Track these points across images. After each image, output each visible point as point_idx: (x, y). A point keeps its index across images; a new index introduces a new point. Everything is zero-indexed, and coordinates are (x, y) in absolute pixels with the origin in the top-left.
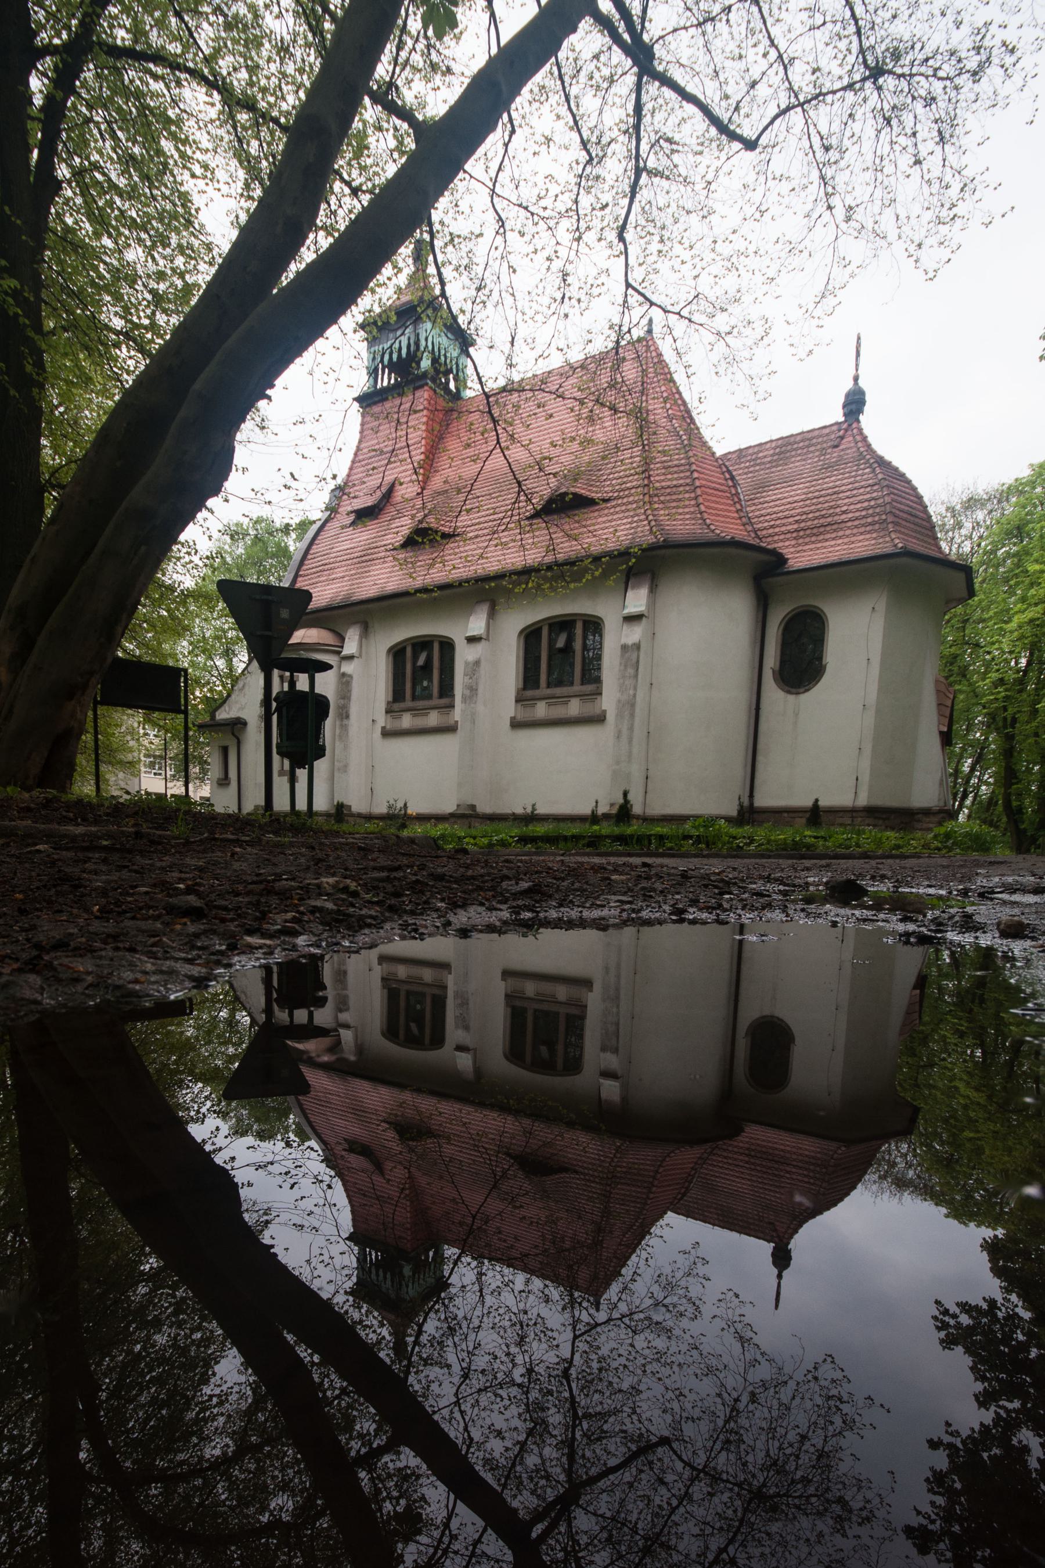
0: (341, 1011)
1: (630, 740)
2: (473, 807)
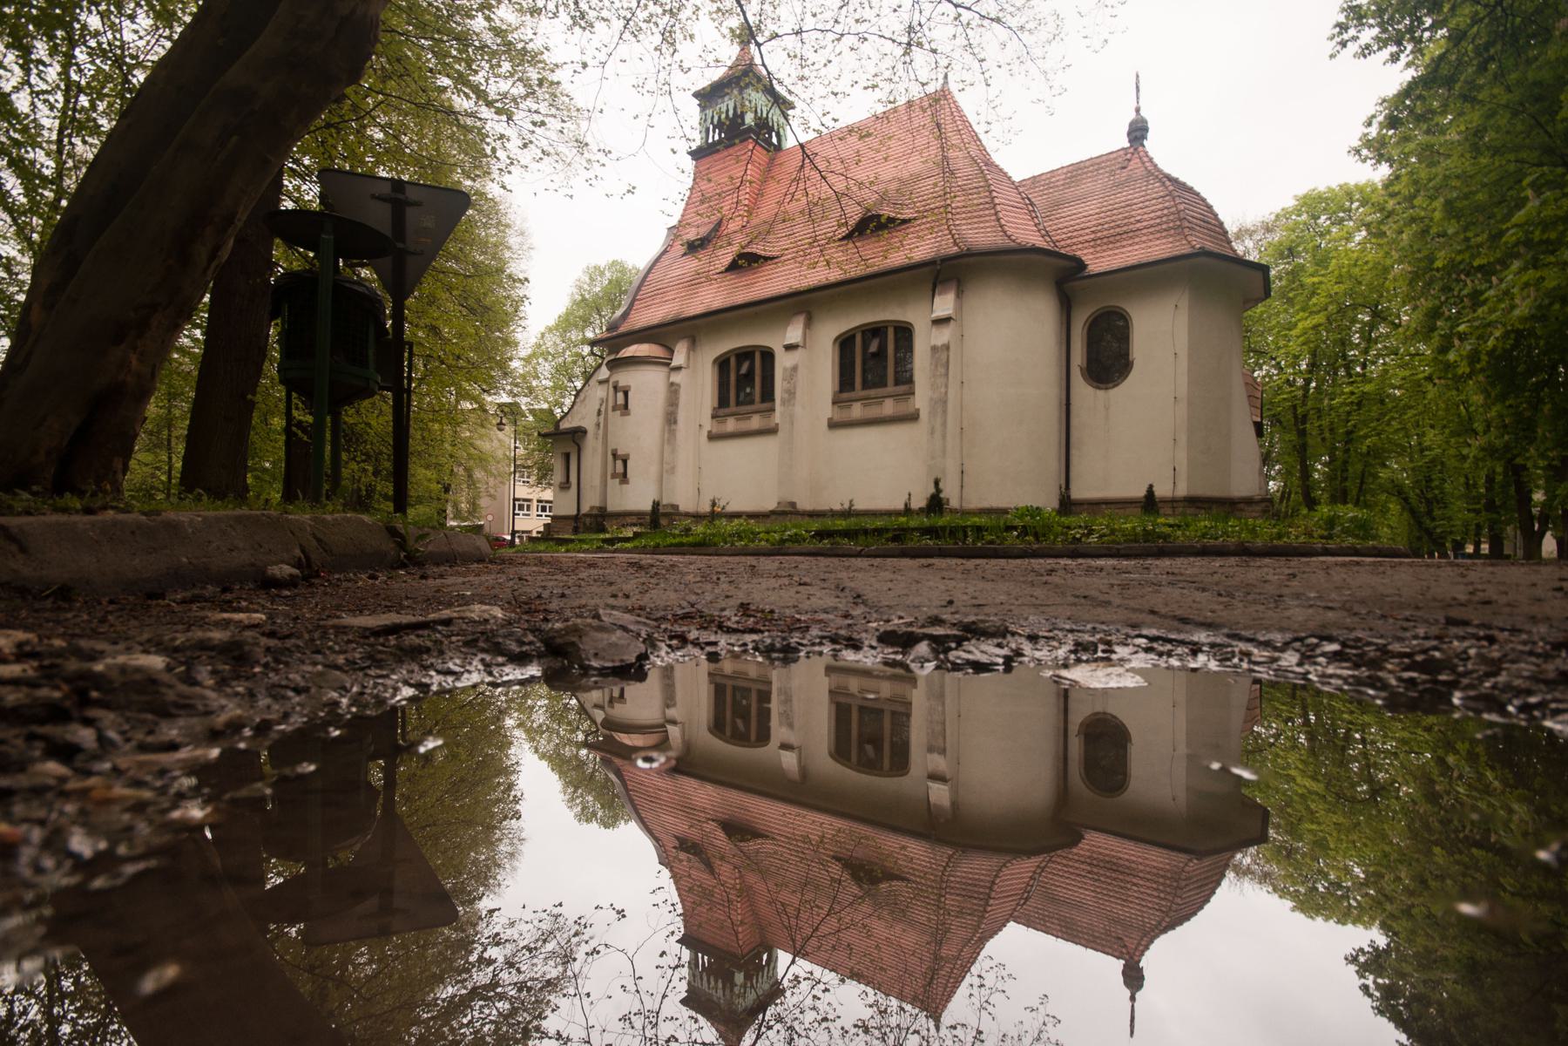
0: (668, 706)
1: (944, 437)
2: (793, 504)
